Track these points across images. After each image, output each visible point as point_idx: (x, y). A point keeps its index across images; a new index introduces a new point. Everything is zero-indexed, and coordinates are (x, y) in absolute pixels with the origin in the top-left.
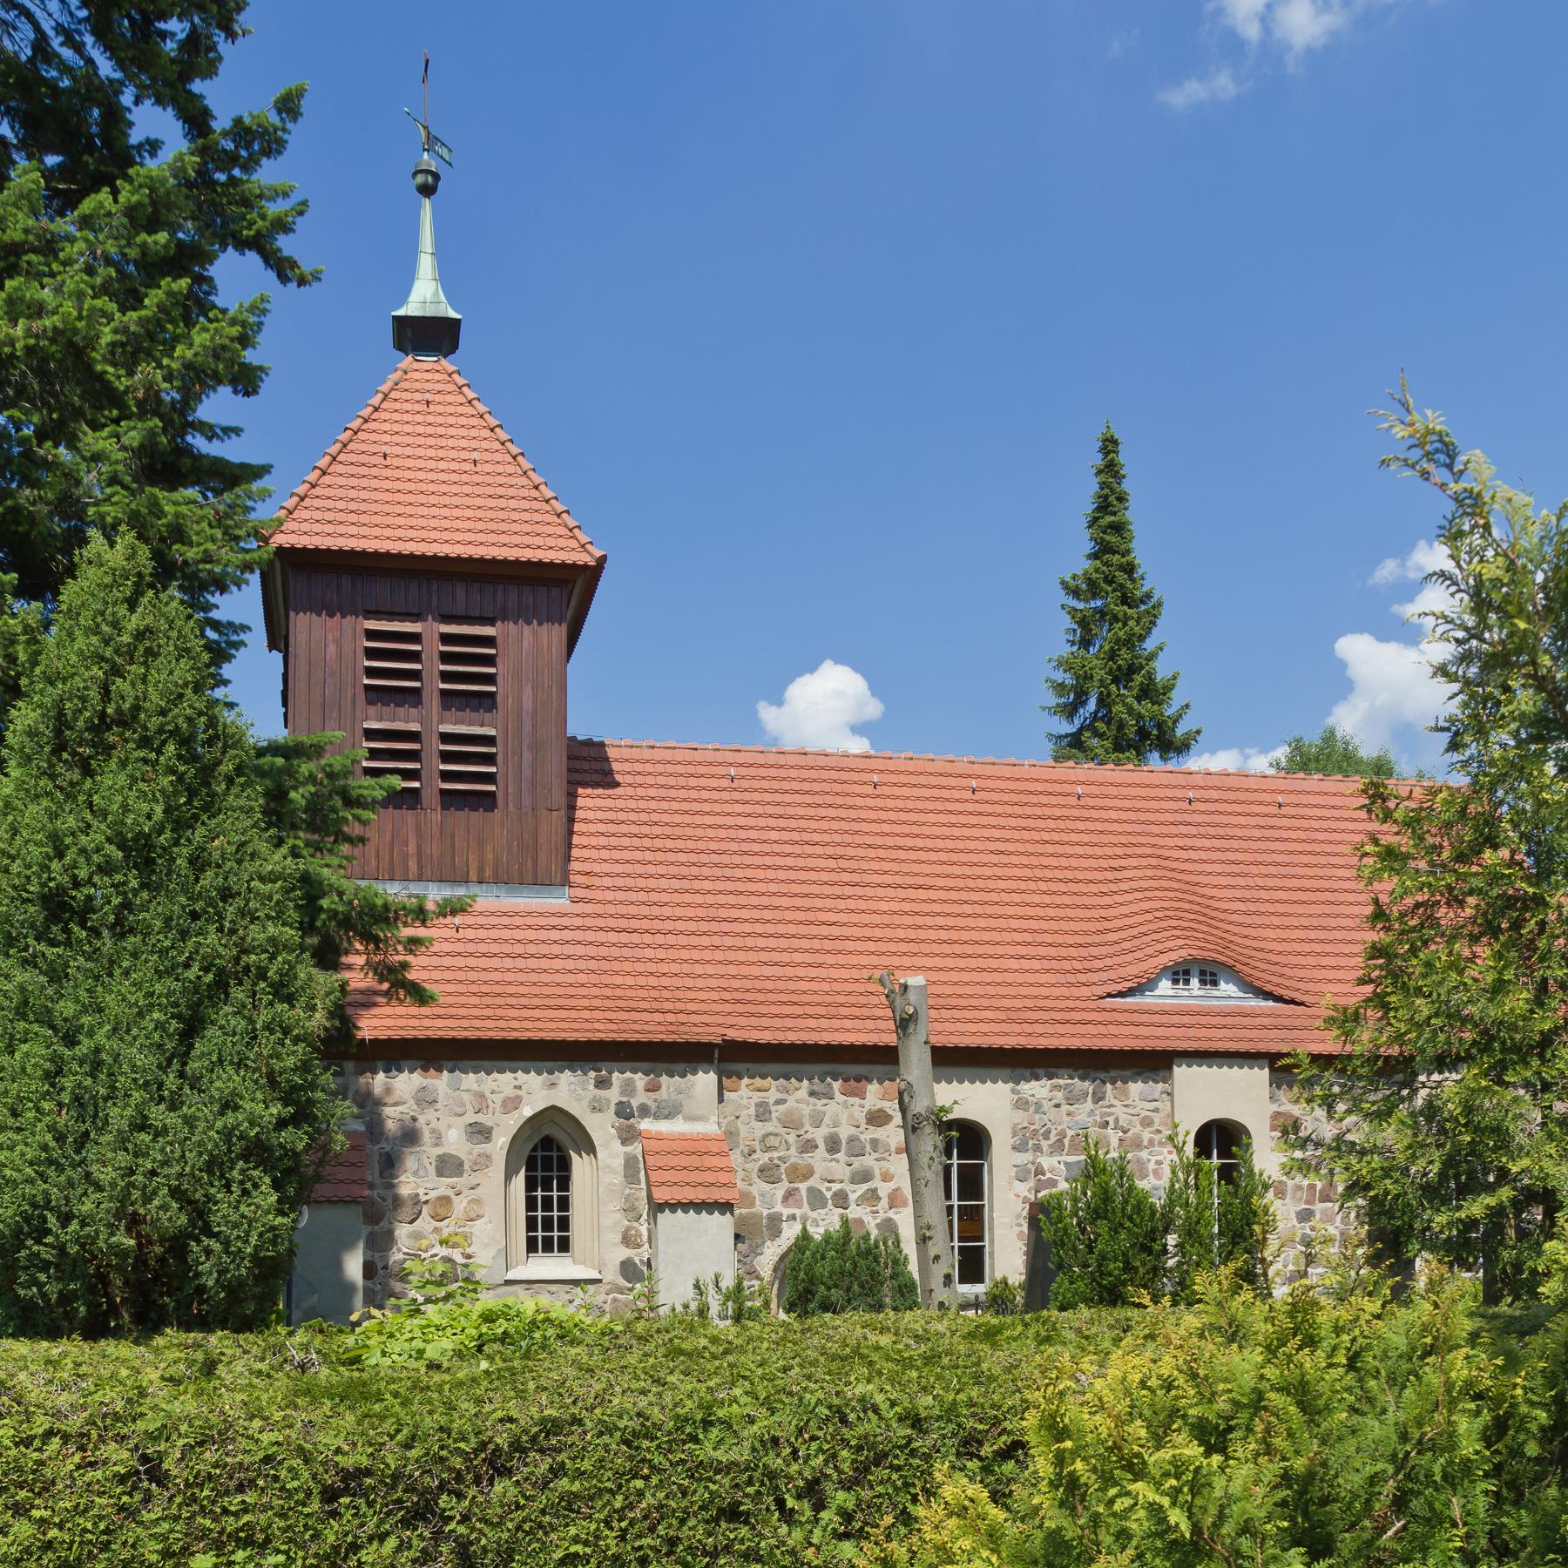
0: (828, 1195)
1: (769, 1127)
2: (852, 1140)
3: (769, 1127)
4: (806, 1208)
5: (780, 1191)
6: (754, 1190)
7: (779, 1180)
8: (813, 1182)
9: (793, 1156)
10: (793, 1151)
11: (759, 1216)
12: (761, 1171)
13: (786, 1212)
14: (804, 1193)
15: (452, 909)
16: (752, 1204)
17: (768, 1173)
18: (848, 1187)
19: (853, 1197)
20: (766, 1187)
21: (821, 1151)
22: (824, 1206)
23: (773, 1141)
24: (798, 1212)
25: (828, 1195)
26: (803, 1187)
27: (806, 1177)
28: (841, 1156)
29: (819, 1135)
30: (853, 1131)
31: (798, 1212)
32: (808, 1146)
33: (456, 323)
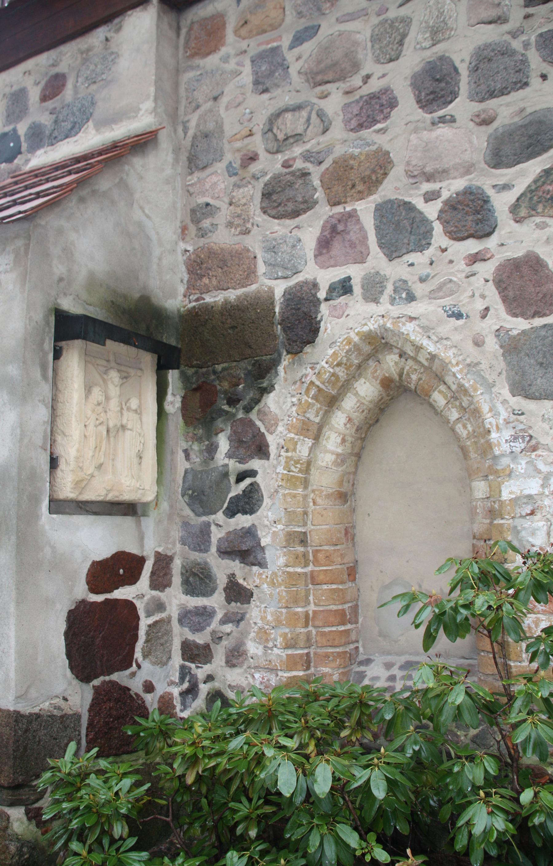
0: (431, 211)
1: (284, 97)
2: (483, 58)
3: (284, 97)
4: (377, 259)
5: (309, 231)
6: (254, 244)
7: (308, 205)
8: (390, 189)
9: (340, 141)
10: (338, 132)
11: (261, 305)
12: (267, 195)
13: (326, 277)
14: (368, 221)
15: (202, 667)
16: (250, 275)
17: (283, 199)
18: (487, 180)
19: (501, 203)
20: (279, 228)
21: (407, 108)
22: (422, 241)
23: (291, 123)
24: (356, 273)
25: (431, 211)
26: (365, 209)
27: (372, 183)
28: (462, 107)
29: (398, 76)
30: (490, 34)
31: (356, 273)
32: (375, 108)
33: (179, 350)
